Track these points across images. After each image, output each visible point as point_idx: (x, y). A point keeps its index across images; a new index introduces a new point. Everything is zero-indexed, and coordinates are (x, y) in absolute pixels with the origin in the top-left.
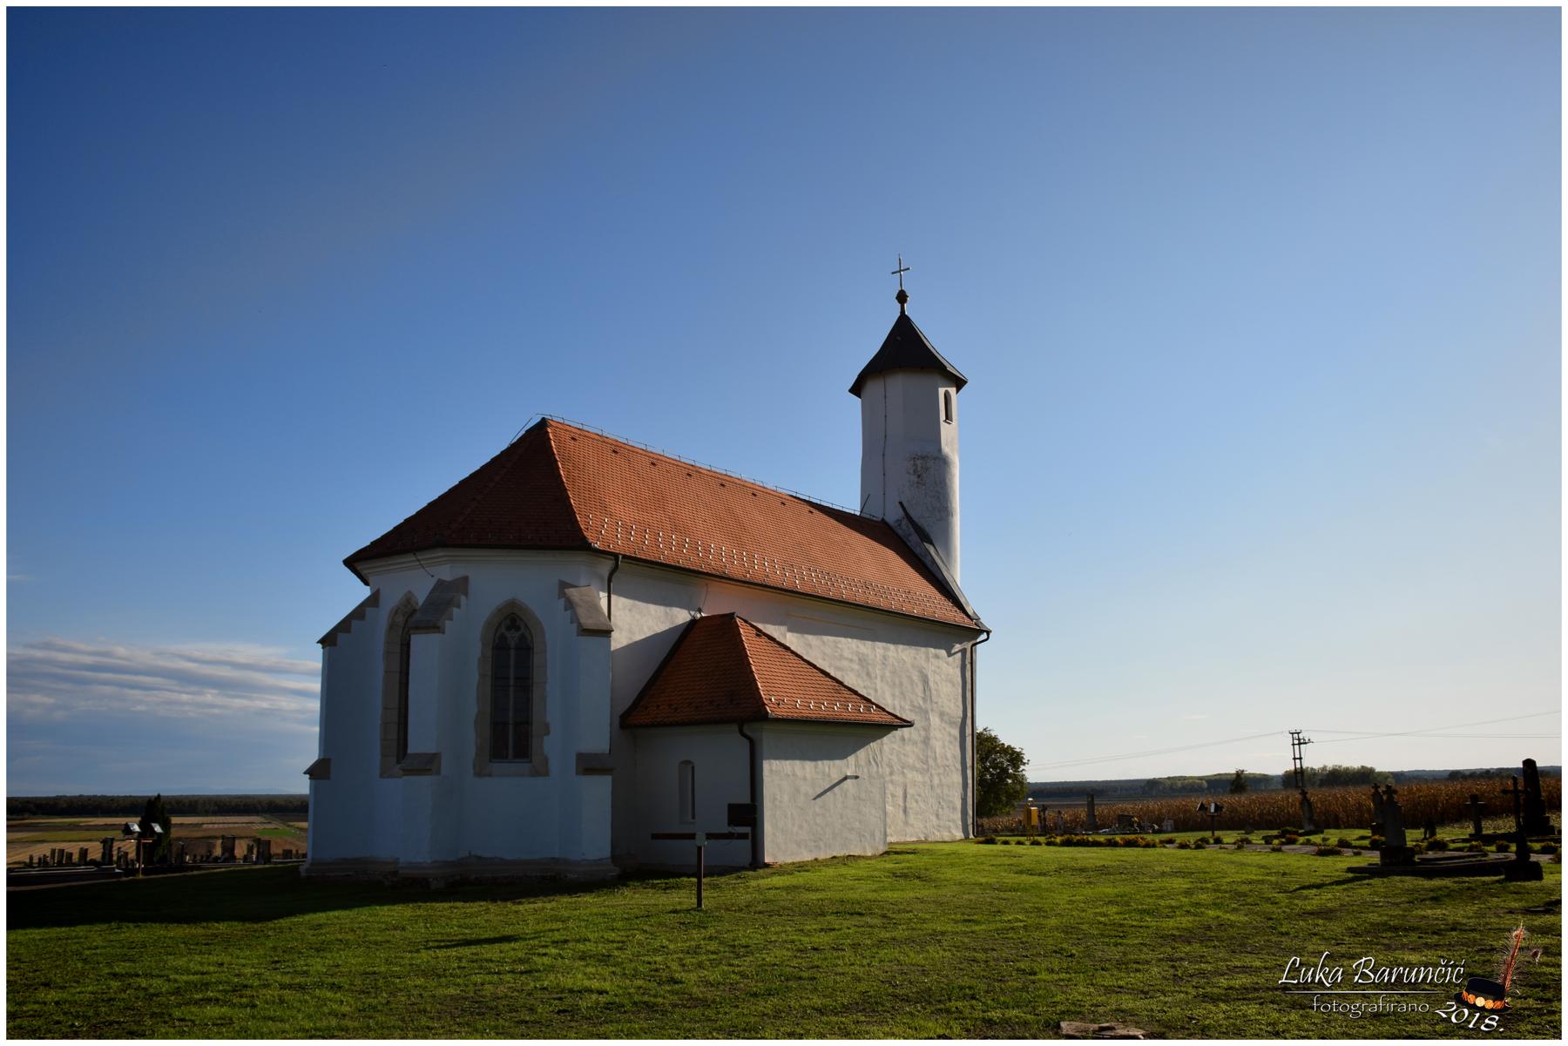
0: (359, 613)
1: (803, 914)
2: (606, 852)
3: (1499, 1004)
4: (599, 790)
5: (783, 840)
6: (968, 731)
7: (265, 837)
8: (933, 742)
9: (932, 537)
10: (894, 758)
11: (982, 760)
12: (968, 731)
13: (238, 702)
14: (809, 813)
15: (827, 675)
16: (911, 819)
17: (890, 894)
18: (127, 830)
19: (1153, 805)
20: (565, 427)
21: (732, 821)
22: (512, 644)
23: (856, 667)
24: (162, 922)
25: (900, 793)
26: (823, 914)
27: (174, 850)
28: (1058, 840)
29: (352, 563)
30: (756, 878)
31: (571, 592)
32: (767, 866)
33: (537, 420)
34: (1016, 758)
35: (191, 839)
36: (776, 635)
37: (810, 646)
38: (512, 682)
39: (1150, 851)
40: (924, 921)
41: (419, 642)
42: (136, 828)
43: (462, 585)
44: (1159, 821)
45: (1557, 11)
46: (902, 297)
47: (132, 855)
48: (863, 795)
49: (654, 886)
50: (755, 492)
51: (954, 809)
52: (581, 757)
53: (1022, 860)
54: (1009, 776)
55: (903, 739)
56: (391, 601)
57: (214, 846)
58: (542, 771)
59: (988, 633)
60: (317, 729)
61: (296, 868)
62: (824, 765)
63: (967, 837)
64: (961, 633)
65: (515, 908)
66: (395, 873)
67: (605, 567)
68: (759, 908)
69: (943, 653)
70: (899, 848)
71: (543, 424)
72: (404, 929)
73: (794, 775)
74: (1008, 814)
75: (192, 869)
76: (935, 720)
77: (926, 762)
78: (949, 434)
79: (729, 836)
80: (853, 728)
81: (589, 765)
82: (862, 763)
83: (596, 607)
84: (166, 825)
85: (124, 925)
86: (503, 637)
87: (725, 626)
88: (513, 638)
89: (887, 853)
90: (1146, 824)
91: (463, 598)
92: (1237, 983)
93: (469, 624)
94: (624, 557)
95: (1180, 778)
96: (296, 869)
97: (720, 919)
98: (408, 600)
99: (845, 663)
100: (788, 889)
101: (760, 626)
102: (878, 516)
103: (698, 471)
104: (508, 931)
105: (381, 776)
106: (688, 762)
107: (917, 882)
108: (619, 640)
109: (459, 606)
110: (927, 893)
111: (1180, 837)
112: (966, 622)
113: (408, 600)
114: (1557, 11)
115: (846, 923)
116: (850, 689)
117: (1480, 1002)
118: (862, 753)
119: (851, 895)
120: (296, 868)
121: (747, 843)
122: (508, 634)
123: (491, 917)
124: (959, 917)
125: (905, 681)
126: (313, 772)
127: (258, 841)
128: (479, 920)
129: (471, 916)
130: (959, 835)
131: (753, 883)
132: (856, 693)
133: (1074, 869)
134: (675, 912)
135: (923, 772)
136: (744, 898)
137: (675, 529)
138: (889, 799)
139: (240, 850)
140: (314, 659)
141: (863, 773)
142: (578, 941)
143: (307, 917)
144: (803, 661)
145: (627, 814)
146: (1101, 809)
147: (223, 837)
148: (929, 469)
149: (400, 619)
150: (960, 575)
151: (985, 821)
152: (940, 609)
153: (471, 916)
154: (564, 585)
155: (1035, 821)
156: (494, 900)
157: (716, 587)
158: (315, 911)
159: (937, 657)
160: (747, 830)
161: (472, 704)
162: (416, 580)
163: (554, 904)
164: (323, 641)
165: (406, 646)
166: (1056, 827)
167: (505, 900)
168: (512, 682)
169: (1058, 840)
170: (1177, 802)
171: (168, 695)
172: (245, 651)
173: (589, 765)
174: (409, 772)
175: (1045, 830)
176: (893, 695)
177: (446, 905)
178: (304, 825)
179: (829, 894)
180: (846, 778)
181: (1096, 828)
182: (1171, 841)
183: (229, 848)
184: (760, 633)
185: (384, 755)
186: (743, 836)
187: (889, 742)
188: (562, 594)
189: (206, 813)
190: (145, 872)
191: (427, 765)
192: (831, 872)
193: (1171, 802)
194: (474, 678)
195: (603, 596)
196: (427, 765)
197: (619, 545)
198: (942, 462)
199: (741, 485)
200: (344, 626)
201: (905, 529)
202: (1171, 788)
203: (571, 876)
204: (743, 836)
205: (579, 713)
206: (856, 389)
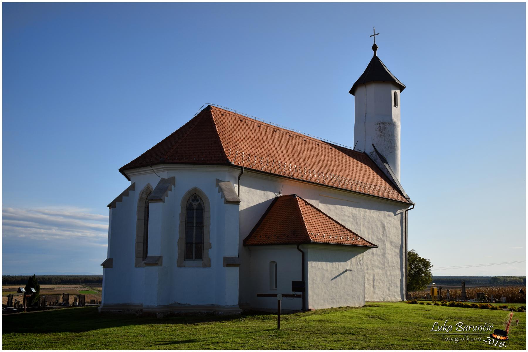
0: (126, 193)
1: (326, 333)
2: (236, 302)
3: (505, 338)
4: (234, 273)
5: (318, 297)
6: (404, 250)
7: (83, 294)
8: (387, 255)
9: (387, 160)
10: (369, 262)
11: (410, 264)
12: (404, 250)
13: (67, 233)
14: (328, 285)
15: (338, 223)
16: (377, 291)
17: (367, 325)
18: (19, 291)
19: (495, 289)
20: (219, 110)
21: (294, 289)
22: (195, 208)
23: (351, 220)
24: (34, 333)
25: (371, 279)
26: (336, 334)
27: (41, 300)
28: (448, 303)
29: (122, 170)
30: (305, 316)
31: (221, 184)
32: (310, 310)
33: (206, 106)
34: (426, 264)
35: (49, 295)
36: (314, 205)
37: (330, 210)
38: (195, 225)
39: (494, 311)
40: (383, 339)
41: (153, 206)
42: (24, 290)
43: (172, 181)
44: (499, 297)
45: (524, 4)
46: (375, 48)
47: (21, 303)
48: (354, 279)
49: (258, 318)
50: (305, 139)
51: (397, 287)
52: (225, 259)
53: (430, 312)
54: (423, 272)
55: (373, 253)
56: (140, 188)
57: (59, 298)
58: (208, 265)
59: (414, 205)
60: (106, 245)
61: (97, 308)
62: (336, 265)
63: (403, 300)
64: (406, 205)
65: (195, 327)
66: (141, 310)
67: (237, 173)
68: (306, 330)
69: (392, 214)
70: (371, 304)
71: (209, 108)
72: (145, 336)
73: (322, 269)
74: (423, 290)
75: (49, 308)
76: (388, 245)
77: (384, 264)
78: (396, 112)
79: (293, 296)
80: (351, 247)
81: (229, 263)
82: (354, 264)
83: (233, 191)
84: (37, 289)
85: (17, 334)
86: (191, 205)
87: (291, 200)
88: (195, 204)
89: (365, 306)
90: (492, 298)
91: (173, 187)
93: (176, 198)
94: (246, 168)
95: (509, 277)
96: (96, 308)
97: (288, 334)
98: (148, 187)
99: (346, 218)
100: (320, 321)
101: (307, 200)
102: (362, 150)
103: (279, 129)
104: (192, 337)
105: (136, 266)
106: (274, 262)
107: (380, 320)
108: (243, 206)
109: (171, 190)
110: (384, 325)
111: (510, 305)
112: (403, 200)
113: (148, 187)
114: (524, 4)
115: (346, 338)
116: (361, 238)
117: (498, 337)
118: (354, 259)
119: (349, 325)
120: (97, 308)
121: (300, 299)
122: (193, 203)
123: (184, 331)
124: (400, 338)
125: (374, 226)
126: (104, 265)
127: (79, 296)
128: (179, 332)
129: (175, 330)
130: (399, 299)
131: (303, 318)
132: (351, 231)
133: (455, 318)
134: (268, 330)
135: (382, 269)
136: (299, 325)
137: (269, 155)
138: (366, 281)
139: (71, 300)
140: (106, 213)
141: (354, 269)
142: (223, 343)
143: (101, 330)
144: (326, 216)
145: (246, 283)
146: (469, 290)
147: (63, 294)
148: (387, 128)
149: (145, 196)
150: (400, 178)
151: (411, 293)
152: (392, 194)
153: (175, 330)
154: (218, 181)
155: (436, 294)
156: (186, 323)
157: (287, 182)
158: (105, 327)
159: (389, 216)
160: (300, 293)
161: (177, 234)
162: (152, 178)
163: (212, 325)
164: (109, 206)
165: (147, 208)
166: (446, 297)
167: (190, 323)
168: (195, 225)
169: (448, 303)
170: (508, 288)
171: (35, 230)
172: (70, 210)
173: (229, 263)
174: (148, 265)
175: (441, 299)
176: (368, 233)
177: (164, 325)
178: (101, 289)
179: (338, 324)
180: (346, 271)
181: (466, 299)
182: (505, 307)
183: (66, 300)
184: (307, 203)
185: (137, 257)
186: (299, 296)
187: (367, 255)
188: (217, 185)
189: (56, 283)
190: (27, 310)
191: (156, 261)
192: (339, 314)
193: (504, 288)
194: (178, 223)
195: (236, 186)
196: (156, 261)
197: (244, 163)
198: (393, 125)
199: (299, 136)
200: (119, 199)
201: (374, 157)
202: (504, 282)
203: (220, 313)
204: (299, 296)
205: (225, 238)
206: (352, 92)
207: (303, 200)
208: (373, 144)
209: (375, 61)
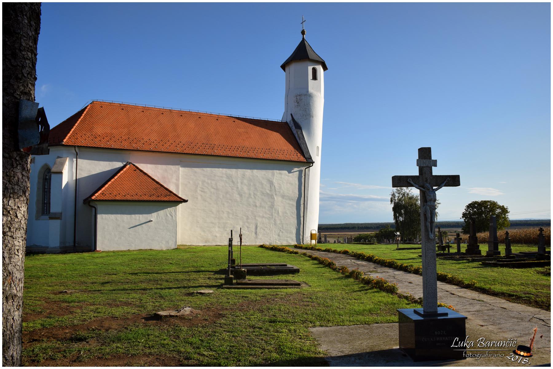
3: (529, 354)
5: (104, 242)
9: (302, 126)
46: (303, 33)
51: (291, 233)
92: (118, 312)
101: (136, 164)
117: (522, 353)
187: (181, 206)
207: (134, 165)
208: (291, 114)
209: (303, 42)
